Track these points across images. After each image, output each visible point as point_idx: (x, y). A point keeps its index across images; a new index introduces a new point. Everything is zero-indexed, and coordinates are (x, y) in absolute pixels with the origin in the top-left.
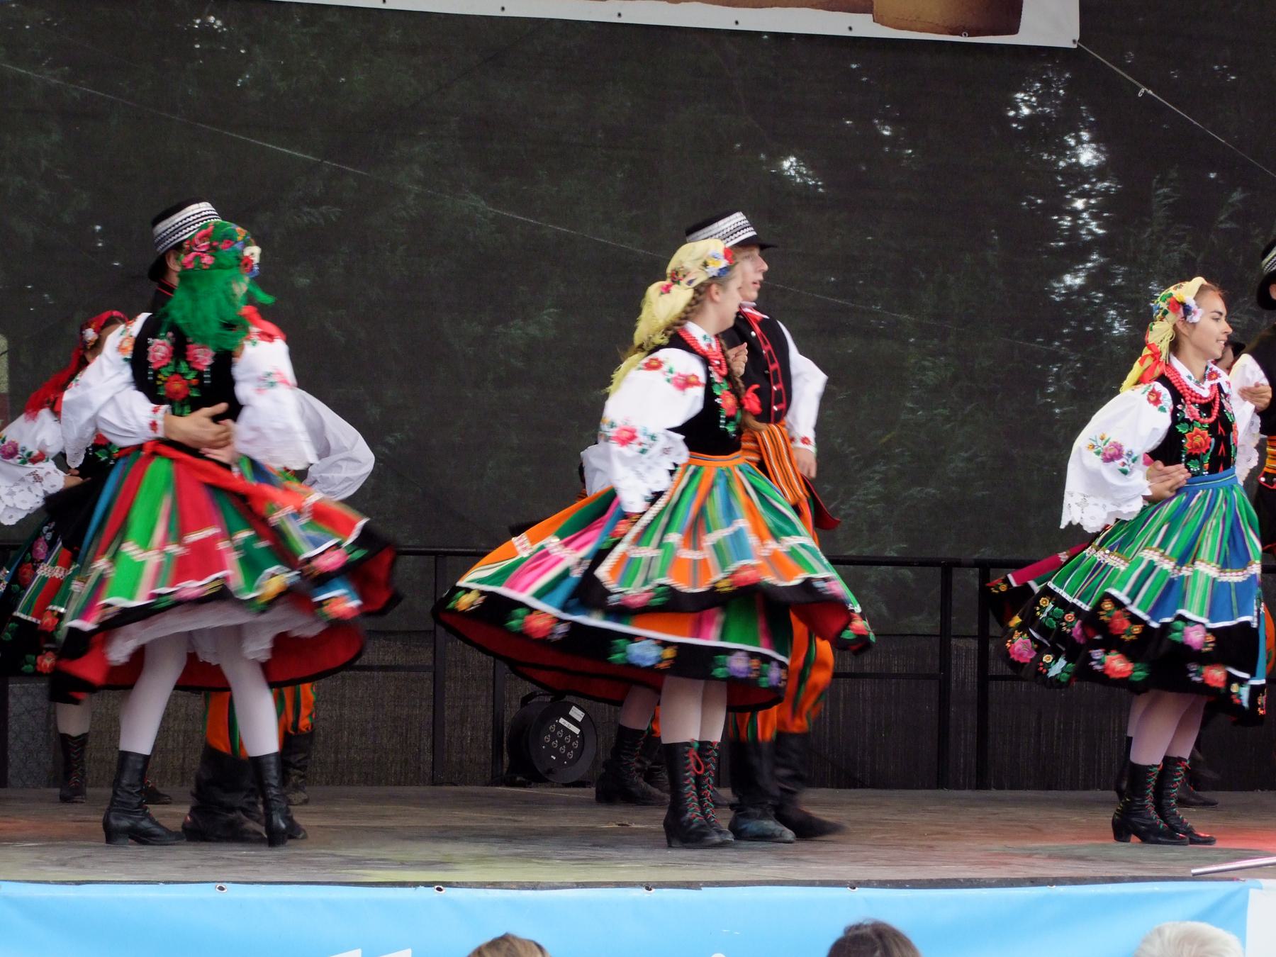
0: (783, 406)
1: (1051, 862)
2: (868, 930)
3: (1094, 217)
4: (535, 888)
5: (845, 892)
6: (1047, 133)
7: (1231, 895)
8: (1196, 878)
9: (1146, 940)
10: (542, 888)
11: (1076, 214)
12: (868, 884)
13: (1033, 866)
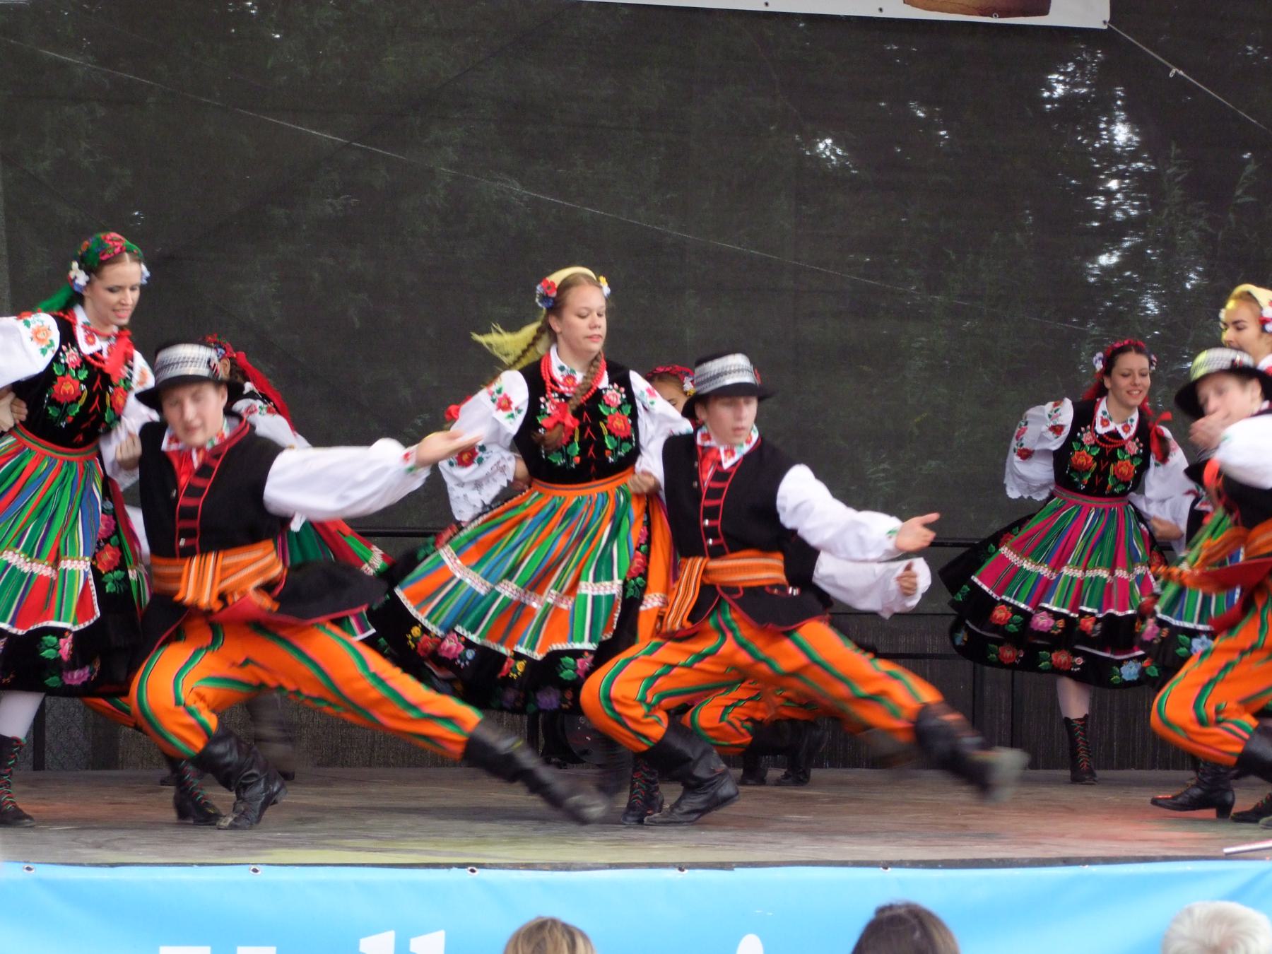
2: (902, 911)
5: (877, 872)
6: (1084, 114)
7: (1262, 875)
8: (1229, 857)
9: (1177, 920)
10: (575, 870)
11: (1109, 194)
12: (900, 864)
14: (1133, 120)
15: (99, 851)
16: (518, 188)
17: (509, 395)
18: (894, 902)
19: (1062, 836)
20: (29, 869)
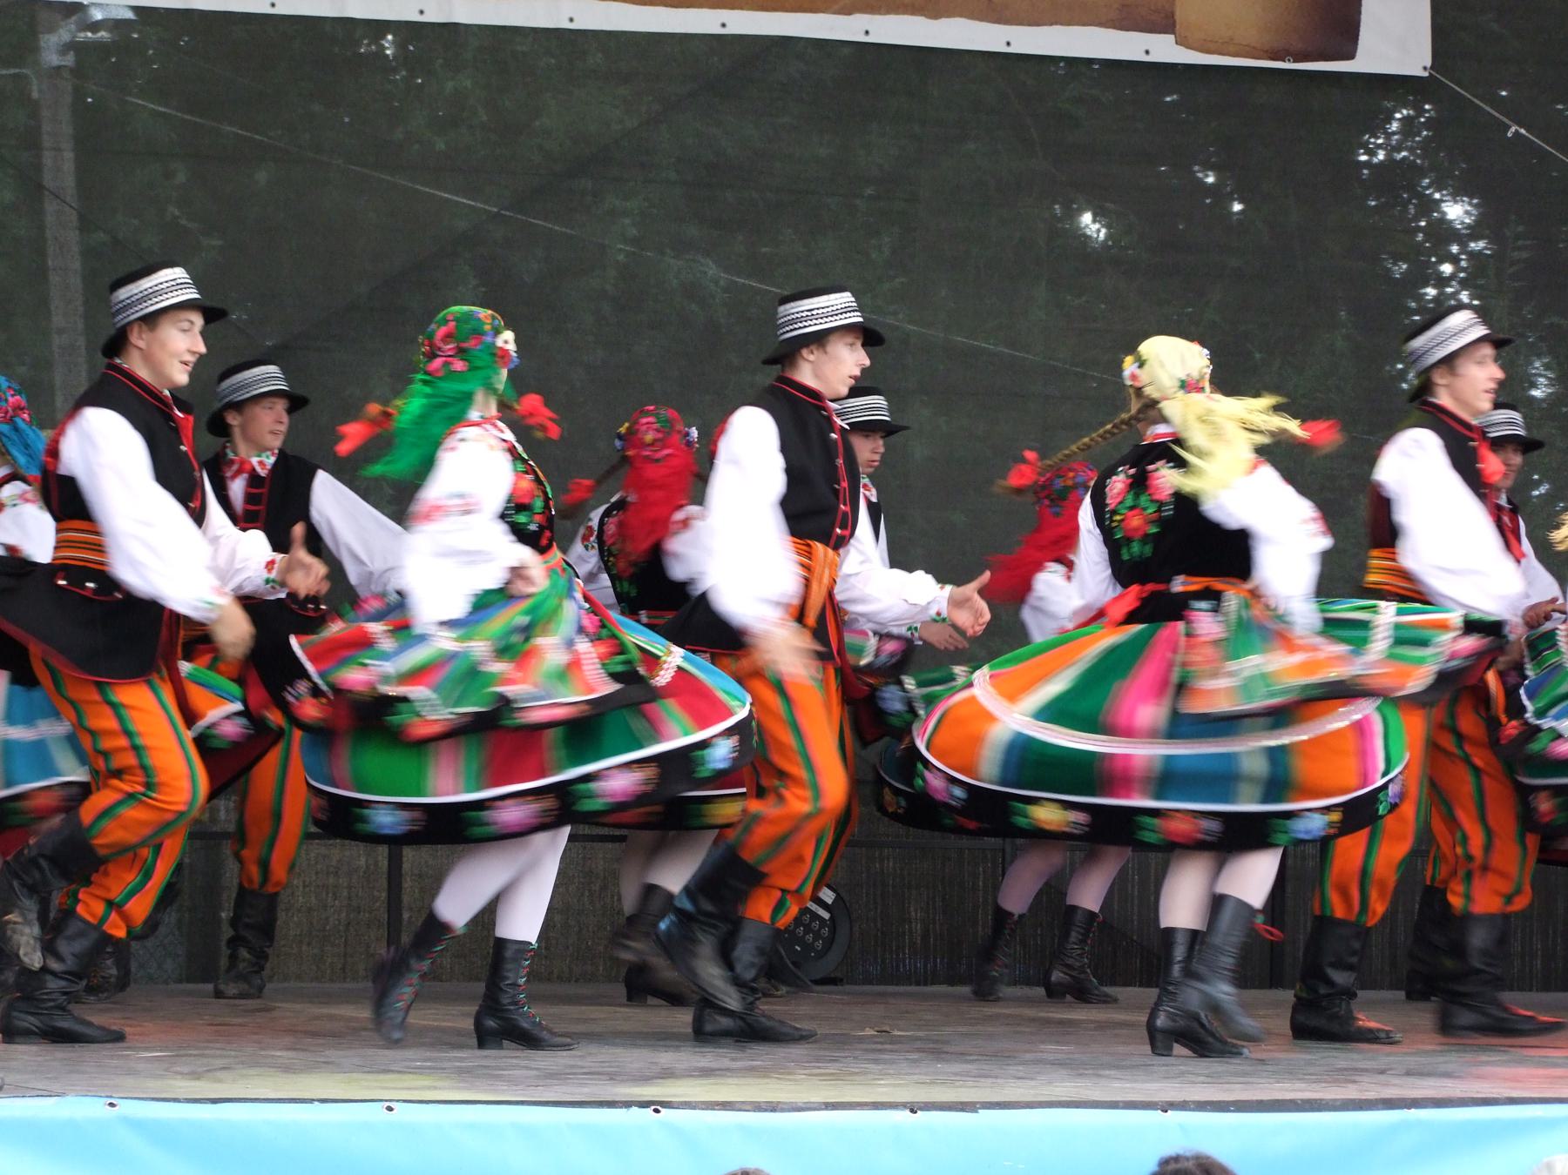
0: (847, 533)
1: (1410, 1080)
2: (1190, 1165)
3: (1464, 284)
4: (774, 1110)
5: (1157, 1115)
10: (783, 1110)
12: (1183, 1106)
13: (1387, 1085)
14: (1456, 196)
15: (197, 1083)
16: (712, 269)
17: (398, 588)
18: (1181, 1152)
19: (1382, 1072)
20: (111, 1105)
